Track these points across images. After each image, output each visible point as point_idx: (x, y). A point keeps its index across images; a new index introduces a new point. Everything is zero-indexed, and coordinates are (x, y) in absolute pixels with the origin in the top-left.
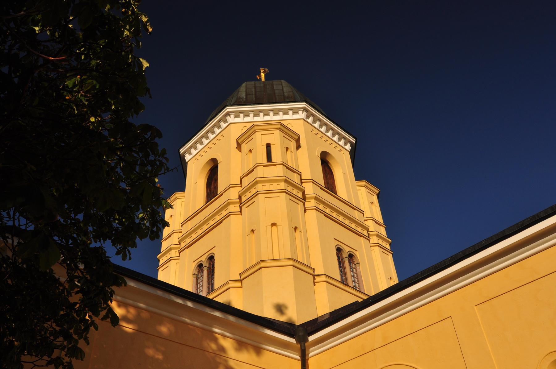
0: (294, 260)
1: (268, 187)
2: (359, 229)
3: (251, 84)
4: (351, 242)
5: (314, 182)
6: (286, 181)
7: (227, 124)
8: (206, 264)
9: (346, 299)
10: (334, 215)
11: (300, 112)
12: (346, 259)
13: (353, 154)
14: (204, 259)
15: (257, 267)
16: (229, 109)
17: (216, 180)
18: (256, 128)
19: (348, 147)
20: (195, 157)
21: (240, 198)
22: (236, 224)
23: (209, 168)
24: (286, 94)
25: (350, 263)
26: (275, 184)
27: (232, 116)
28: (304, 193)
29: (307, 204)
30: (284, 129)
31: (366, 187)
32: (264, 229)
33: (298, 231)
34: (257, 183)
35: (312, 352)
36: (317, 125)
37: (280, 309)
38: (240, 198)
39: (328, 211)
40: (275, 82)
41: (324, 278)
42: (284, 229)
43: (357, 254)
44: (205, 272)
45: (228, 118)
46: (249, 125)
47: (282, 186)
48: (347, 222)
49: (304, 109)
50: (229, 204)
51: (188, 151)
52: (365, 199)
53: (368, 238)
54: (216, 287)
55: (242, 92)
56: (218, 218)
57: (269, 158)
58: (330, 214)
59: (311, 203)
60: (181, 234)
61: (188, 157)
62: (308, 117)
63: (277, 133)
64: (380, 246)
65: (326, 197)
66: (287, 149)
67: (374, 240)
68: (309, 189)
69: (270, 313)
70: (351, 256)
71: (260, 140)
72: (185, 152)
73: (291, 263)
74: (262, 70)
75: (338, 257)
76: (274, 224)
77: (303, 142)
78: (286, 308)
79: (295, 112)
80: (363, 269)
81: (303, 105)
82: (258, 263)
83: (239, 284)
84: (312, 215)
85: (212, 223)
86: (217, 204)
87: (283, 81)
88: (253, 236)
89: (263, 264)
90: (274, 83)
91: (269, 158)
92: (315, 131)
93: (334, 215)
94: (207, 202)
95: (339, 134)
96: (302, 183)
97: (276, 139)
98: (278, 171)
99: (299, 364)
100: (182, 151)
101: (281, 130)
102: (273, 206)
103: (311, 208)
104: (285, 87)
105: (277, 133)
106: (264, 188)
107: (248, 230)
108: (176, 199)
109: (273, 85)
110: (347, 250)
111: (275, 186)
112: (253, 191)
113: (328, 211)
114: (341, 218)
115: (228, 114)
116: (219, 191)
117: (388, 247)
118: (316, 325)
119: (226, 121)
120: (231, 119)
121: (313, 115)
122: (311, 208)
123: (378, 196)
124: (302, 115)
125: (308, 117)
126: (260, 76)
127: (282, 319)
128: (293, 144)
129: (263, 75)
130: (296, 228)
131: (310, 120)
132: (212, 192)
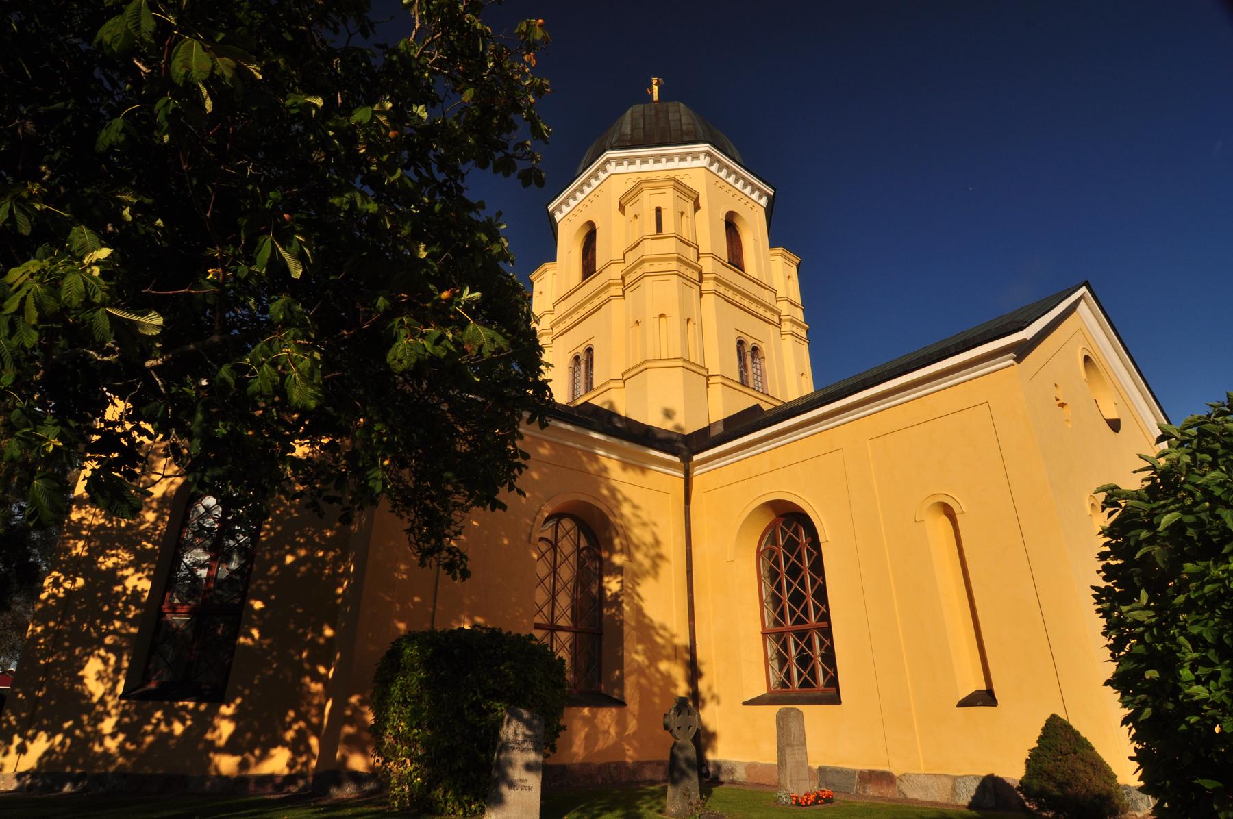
0: (685, 360)
1: (656, 267)
2: (768, 315)
3: (638, 108)
4: (756, 331)
5: (715, 257)
6: (679, 260)
7: (606, 175)
8: (583, 357)
9: (743, 402)
10: (738, 298)
11: (702, 157)
12: (747, 353)
13: (770, 211)
14: (581, 350)
15: (641, 368)
16: (610, 154)
17: (594, 249)
18: (643, 185)
19: (764, 201)
20: (569, 213)
21: (623, 278)
22: (617, 311)
23: (585, 233)
24: (684, 128)
25: (753, 357)
26: (665, 263)
27: (613, 164)
28: (700, 273)
29: (704, 287)
30: (679, 187)
31: (783, 256)
32: (650, 322)
33: (691, 324)
34: (643, 262)
35: (697, 471)
36: (723, 174)
37: (668, 414)
38: (623, 278)
39: (730, 294)
40: (670, 104)
41: (719, 379)
42: (674, 321)
43: (763, 347)
44: (583, 367)
45: (608, 166)
46: (635, 178)
47: (674, 265)
48: (753, 307)
49: (708, 154)
50: (609, 285)
51: (559, 208)
52: (776, 272)
53: (778, 325)
54: (595, 385)
55: (626, 126)
56: (596, 302)
57: (659, 228)
58: (732, 299)
59: (708, 285)
60: (553, 317)
61: (558, 216)
62: (711, 164)
63: (670, 192)
64: (794, 334)
65: (730, 275)
66: (682, 213)
67: (786, 326)
68: (707, 265)
69: (654, 419)
70: (755, 349)
71: (648, 201)
72: (554, 209)
73: (681, 363)
74: (655, 81)
75: (739, 351)
76: (662, 315)
77: (703, 202)
78: (674, 413)
79: (695, 157)
80: (770, 365)
81: (706, 147)
82: (643, 363)
83: (621, 384)
84: (709, 299)
85: (589, 307)
86: (595, 283)
87: (682, 105)
88: (638, 328)
89: (648, 365)
90: (670, 109)
91: (659, 228)
92: (721, 183)
93: (738, 298)
94: (584, 278)
95: (752, 184)
96: (699, 258)
97: (667, 199)
98: (668, 246)
99: (683, 481)
100: (551, 208)
101: (675, 188)
102: (662, 292)
103: (709, 292)
104: (681, 114)
105: (670, 192)
106: (653, 269)
107: (632, 321)
108: (545, 271)
109: (667, 112)
110: (750, 342)
111: (665, 266)
112: (639, 272)
113: (730, 294)
114: (746, 303)
115: (608, 161)
116: (598, 267)
117: (804, 334)
118: (703, 439)
119: (605, 171)
120: (611, 168)
121: (719, 161)
122: (709, 292)
123: (798, 266)
124: (704, 161)
125: (711, 164)
126: (652, 90)
127: (668, 426)
128: (690, 206)
129: (656, 88)
130: (688, 320)
131: (714, 168)
132: (588, 268)
